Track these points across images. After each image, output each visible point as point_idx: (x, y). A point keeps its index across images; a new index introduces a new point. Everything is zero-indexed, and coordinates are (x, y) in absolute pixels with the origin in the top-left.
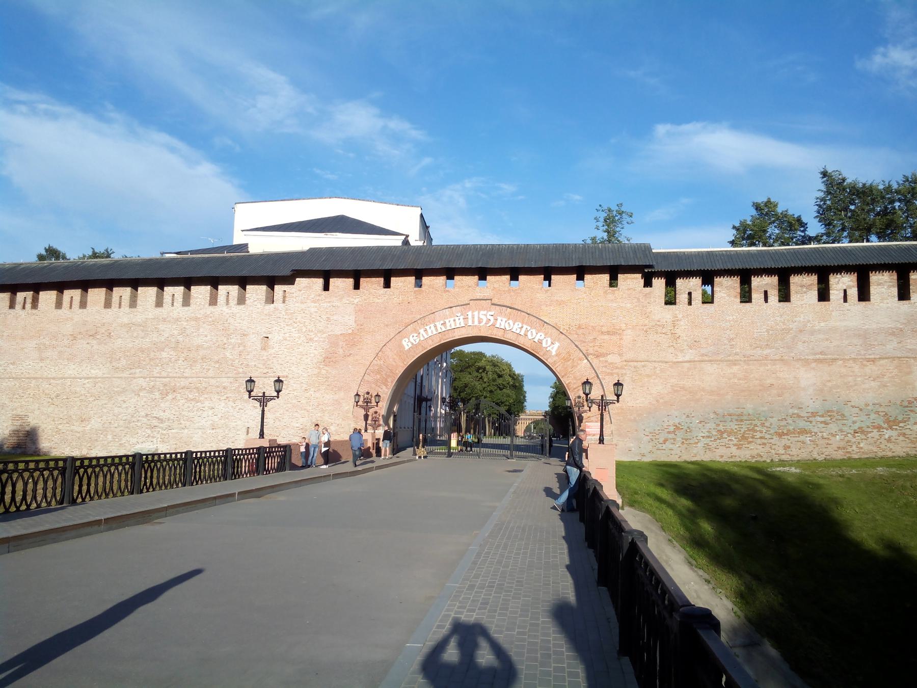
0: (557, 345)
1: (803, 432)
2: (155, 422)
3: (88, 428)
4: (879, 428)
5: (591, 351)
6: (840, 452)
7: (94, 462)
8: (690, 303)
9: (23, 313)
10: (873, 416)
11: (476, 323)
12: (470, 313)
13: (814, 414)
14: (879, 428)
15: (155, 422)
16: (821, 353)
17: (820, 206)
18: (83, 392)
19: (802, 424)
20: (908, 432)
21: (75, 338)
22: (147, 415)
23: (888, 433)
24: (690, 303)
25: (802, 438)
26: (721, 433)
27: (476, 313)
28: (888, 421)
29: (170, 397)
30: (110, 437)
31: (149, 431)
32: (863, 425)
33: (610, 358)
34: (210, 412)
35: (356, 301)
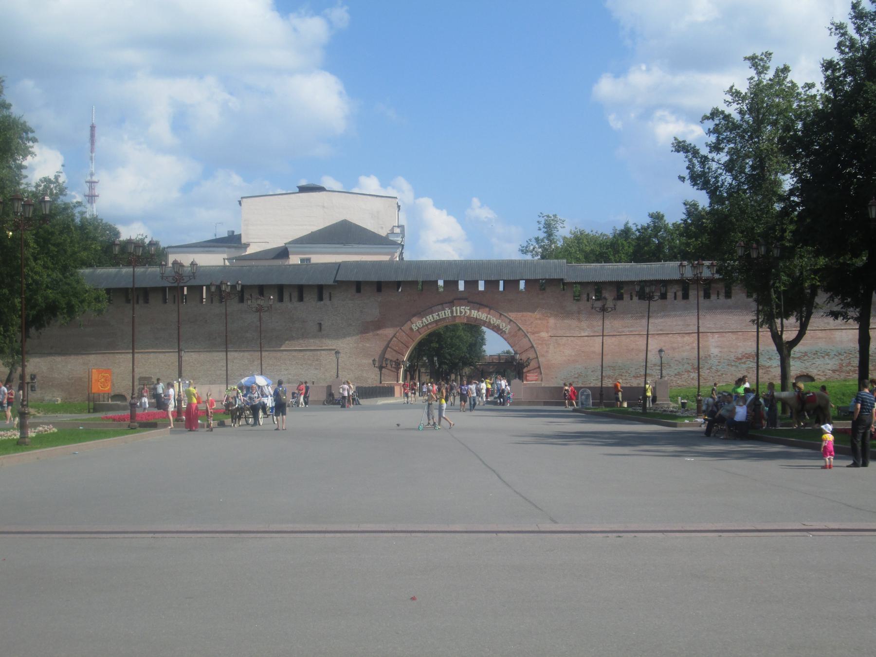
0: (509, 327)
10: (686, 366)
33: (544, 334)
34: (286, 372)
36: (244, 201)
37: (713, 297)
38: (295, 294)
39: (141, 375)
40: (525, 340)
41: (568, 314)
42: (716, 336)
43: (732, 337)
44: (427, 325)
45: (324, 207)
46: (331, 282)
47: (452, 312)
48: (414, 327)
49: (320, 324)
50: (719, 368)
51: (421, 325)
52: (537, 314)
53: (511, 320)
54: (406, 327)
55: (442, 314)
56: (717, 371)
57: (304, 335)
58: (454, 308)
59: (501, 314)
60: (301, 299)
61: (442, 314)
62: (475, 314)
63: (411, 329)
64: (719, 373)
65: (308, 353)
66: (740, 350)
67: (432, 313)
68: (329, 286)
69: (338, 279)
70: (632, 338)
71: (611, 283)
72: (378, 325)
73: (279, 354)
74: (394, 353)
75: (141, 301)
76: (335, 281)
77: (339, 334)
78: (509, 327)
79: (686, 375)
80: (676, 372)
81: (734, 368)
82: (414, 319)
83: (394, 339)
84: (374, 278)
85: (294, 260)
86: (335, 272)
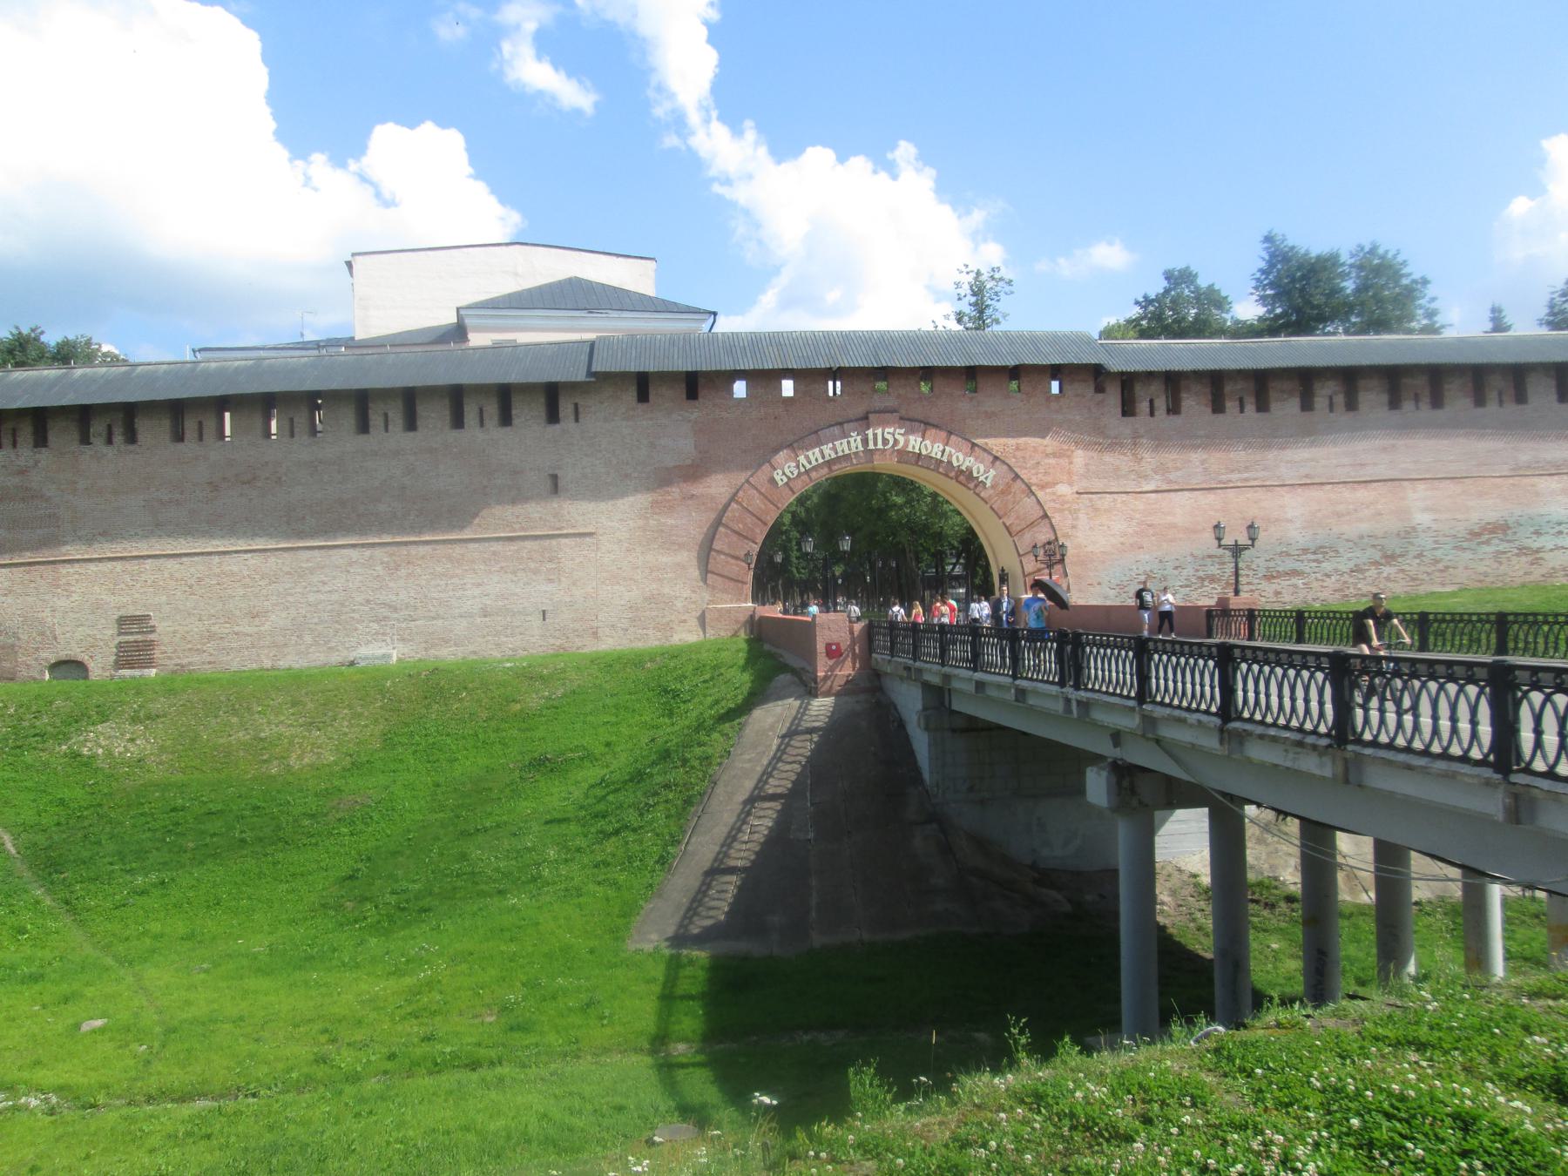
0: (992, 472)
1: (1295, 573)
2: (385, 612)
3: (267, 627)
4: (1376, 563)
5: (1034, 480)
6: (1337, 595)
7: (1531, 618)
8: (1152, 414)
9: (109, 452)
10: (1370, 552)
11: (880, 446)
12: (870, 432)
13: (1305, 551)
14: (1376, 563)
15: (385, 612)
16: (1307, 476)
17: (1258, 280)
18: (246, 573)
19: (1290, 565)
20: (1406, 567)
21: (215, 487)
22: (368, 601)
23: (1387, 570)
24: (1152, 414)
25: (1294, 581)
26: (1202, 579)
27: (879, 431)
28: (1386, 557)
29: (403, 572)
30: (308, 639)
31: (375, 626)
32: (1359, 562)
33: (1063, 489)
34: (477, 592)
35: (693, 417)
36: (358, 263)
37: (1408, 405)
38: (492, 409)
39: (123, 612)
40: (1030, 501)
41: (1114, 445)
42: (1421, 486)
43: (1452, 488)
44: (807, 472)
45: (516, 274)
46: (581, 376)
47: (865, 441)
48: (779, 477)
49: (555, 478)
50: (1438, 553)
51: (795, 470)
52: (1049, 443)
53: (996, 458)
54: (760, 477)
55: (842, 446)
56: (1437, 561)
57: (517, 496)
58: (870, 432)
59: (974, 445)
60: (506, 419)
61: (842, 446)
62: (915, 443)
63: (772, 481)
64: (1440, 566)
65: (528, 544)
66: (1475, 517)
67: (819, 443)
68: (574, 387)
69: (596, 368)
70: (1250, 494)
71: (1198, 375)
72: (694, 471)
73: (458, 550)
74: (735, 538)
75: (118, 438)
76: (590, 373)
77: (599, 491)
78: (992, 472)
79: (1372, 572)
80: (1351, 565)
81: (1468, 555)
82: (782, 455)
83: (734, 505)
84: (682, 363)
85: (477, 339)
86: (585, 358)
